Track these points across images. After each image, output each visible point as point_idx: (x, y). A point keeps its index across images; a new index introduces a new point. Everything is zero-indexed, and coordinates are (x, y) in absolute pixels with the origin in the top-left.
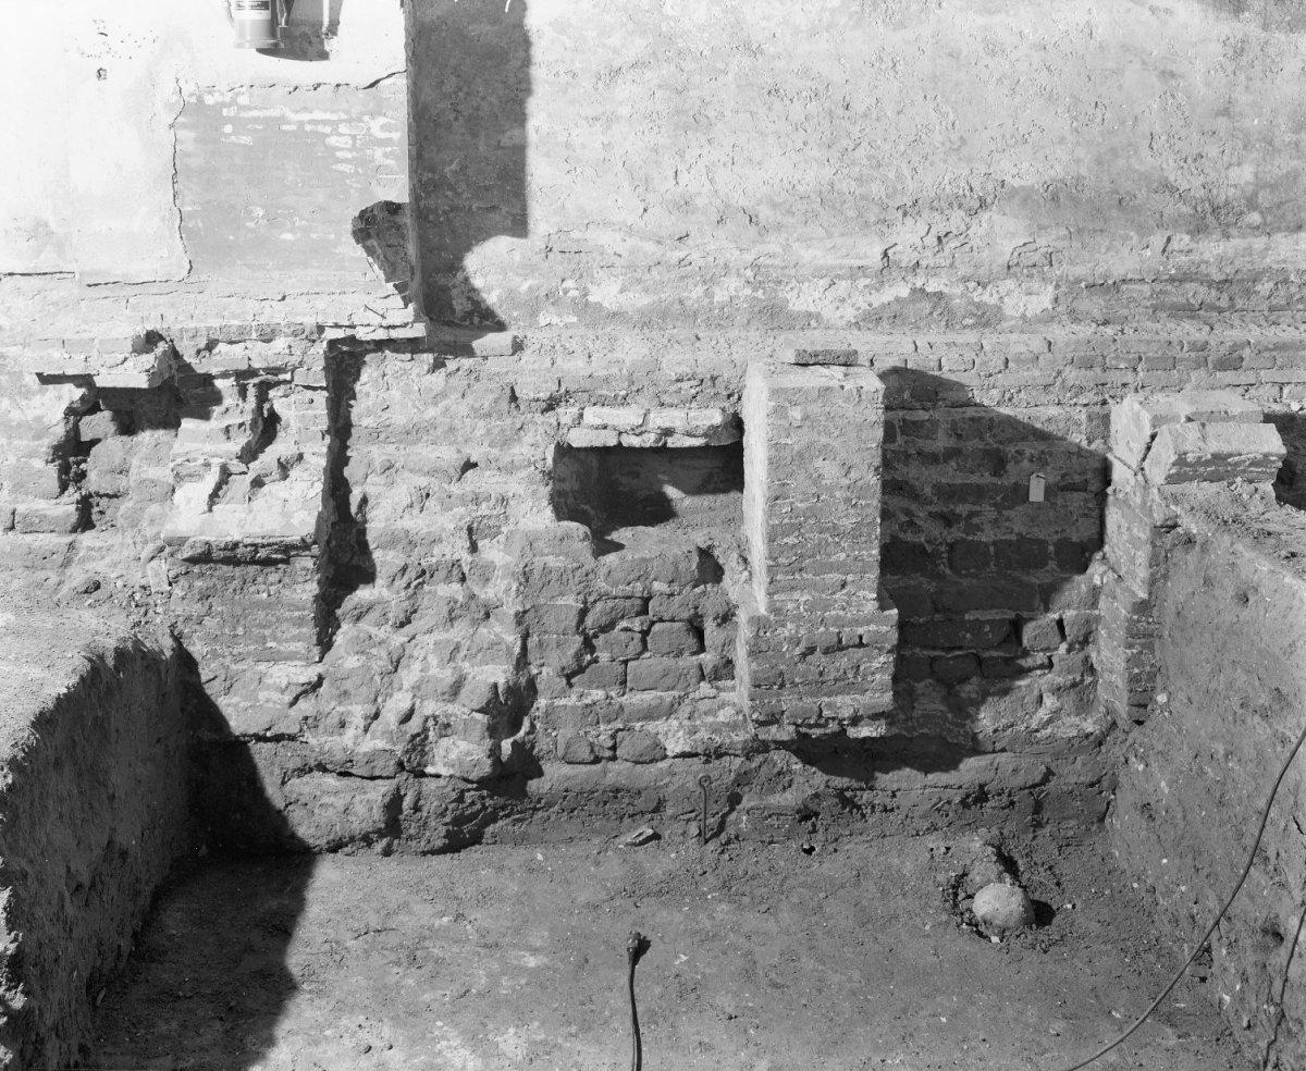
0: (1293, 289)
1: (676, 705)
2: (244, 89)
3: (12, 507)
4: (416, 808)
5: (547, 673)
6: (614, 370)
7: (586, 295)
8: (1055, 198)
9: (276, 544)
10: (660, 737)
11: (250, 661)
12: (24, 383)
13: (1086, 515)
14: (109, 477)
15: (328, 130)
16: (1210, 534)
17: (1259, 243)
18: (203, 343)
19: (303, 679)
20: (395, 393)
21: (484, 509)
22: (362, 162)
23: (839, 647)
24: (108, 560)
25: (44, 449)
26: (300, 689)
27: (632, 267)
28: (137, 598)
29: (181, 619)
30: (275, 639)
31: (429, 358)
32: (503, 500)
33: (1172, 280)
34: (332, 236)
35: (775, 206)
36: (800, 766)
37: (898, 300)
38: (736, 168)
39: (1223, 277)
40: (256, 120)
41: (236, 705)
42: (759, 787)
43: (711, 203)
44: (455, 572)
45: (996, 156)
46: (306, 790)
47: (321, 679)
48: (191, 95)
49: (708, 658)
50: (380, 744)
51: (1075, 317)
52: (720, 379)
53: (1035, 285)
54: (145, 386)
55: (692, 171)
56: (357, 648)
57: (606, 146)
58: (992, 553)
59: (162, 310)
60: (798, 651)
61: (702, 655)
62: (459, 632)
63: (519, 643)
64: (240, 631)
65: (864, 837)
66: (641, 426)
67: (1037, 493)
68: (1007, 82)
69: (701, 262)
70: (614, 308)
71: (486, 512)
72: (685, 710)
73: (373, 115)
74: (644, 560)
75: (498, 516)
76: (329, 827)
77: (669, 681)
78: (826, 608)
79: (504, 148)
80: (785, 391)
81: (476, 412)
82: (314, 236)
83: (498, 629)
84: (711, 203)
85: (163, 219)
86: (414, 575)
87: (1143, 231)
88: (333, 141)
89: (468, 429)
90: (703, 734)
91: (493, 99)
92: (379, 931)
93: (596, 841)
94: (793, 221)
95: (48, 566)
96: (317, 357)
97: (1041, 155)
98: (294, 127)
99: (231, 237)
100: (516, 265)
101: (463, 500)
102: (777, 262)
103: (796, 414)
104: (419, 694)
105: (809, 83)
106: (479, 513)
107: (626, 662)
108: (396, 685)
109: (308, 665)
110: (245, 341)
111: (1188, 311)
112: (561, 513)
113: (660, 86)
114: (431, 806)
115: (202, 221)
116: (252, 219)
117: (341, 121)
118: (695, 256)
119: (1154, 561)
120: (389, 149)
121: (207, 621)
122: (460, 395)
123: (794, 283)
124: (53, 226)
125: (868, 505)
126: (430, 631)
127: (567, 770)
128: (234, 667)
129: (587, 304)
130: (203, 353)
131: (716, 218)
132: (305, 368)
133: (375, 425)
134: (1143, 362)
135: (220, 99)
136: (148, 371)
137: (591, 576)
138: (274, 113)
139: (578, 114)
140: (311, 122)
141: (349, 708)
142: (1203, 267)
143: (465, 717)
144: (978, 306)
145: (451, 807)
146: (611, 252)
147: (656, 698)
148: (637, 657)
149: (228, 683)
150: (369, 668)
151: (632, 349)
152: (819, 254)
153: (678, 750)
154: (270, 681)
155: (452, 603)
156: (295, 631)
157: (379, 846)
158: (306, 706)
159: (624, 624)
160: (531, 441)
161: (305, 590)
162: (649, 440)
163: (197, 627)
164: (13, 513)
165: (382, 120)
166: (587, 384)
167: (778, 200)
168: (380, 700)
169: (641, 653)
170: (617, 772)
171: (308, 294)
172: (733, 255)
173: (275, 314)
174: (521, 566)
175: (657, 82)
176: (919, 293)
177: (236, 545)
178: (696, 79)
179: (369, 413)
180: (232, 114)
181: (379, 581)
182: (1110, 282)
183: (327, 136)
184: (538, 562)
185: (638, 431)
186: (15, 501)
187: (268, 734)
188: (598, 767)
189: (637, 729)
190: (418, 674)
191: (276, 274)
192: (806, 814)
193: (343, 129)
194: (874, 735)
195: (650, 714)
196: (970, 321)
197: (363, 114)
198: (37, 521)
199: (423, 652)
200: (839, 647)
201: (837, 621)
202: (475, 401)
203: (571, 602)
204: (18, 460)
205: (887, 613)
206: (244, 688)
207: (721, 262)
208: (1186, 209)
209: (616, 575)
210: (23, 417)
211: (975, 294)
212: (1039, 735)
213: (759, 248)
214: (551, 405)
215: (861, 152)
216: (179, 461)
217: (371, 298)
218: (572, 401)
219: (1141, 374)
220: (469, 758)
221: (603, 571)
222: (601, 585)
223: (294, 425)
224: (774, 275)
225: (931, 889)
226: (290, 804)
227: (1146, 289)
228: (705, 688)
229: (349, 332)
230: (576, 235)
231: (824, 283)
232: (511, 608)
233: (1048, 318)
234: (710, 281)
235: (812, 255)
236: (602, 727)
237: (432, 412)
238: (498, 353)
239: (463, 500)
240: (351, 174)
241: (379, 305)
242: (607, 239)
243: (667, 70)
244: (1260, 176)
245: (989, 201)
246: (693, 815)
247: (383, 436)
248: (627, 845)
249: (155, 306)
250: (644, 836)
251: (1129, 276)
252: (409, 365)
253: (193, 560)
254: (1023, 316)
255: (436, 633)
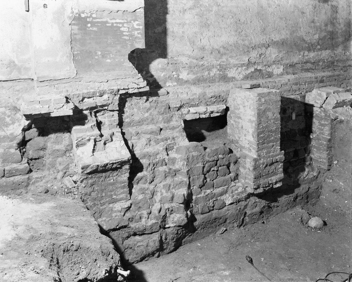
0: (326, 64)
1: (227, 190)
2: (94, 12)
3: (3, 168)
4: (166, 239)
5: (195, 188)
6: (195, 96)
7: (179, 76)
8: (283, 43)
9: (120, 162)
10: (224, 200)
11: (107, 204)
12: (6, 121)
13: (303, 121)
14: (36, 152)
15: (121, 25)
16: (349, 119)
17: (320, 53)
18: (81, 98)
19: (126, 206)
20: (135, 110)
21: (169, 142)
22: (131, 36)
23: (272, 164)
24: (44, 181)
25: (15, 145)
26: (126, 210)
27: (190, 67)
28: (66, 191)
29: (84, 195)
30: (115, 195)
31: (145, 98)
32: (173, 138)
33: (305, 63)
34: (122, 60)
35: (224, 48)
36: (258, 200)
37: (252, 72)
38: (215, 37)
39: (314, 62)
40: (98, 22)
41: (105, 220)
42: (249, 208)
43: (209, 48)
44: (164, 163)
45: (271, 33)
46: (131, 243)
47: (131, 204)
48: (76, 14)
49: (232, 175)
50: (154, 221)
51: (288, 73)
52: (221, 96)
53: (279, 66)
54: (72, 114)
55: (205, 39)
56: (141, 192)
57: (183, 32)
58: (285, 134)
59: (67, 88)
60: (264, 166)
61: (230, 174)
62: (169, 180)
63: (188, 180)
64: (104, 195)
65: (273, 216)
66: (206, 111)
67: (294, 117)
68: (272, 14)
69: (207, 65)
70: (186, 79)
71: (170, 143)
72: (230, 191)
73: (134, 21)
74: (216, 149)
75: (173, 143)
76: (141, 253)
77: (225, 183)
78: (269, 153)
79: (156, 33)
80: (261, 94)
81: (160, 113)
82: (117, 60)
83: (180, 177)
84: (209, 48)
85: (67, 57)
86: (152, 166)
87: (300, 51)
88: (122, 29)
89: (157, 118)
90: (235, 197)
91: (153, 18)
92: (176, 279)
93: (211, 235)
94: (228, 52)
95: (21, 187)
96: (116, 100)
97: (280, 33)
98: (110, 25)
99: (90, 62)
100: (160, 68)
101: (163, 140)
102: (225, 64)
103: (263, 100)
104: (162, 203)
105: (231, 14)
106: (168, 143)
107: (213, 180)
108: (154, 201)
109: (126, 201)
110: (93, 97)
111: (307, 70)
112: (190, 140)
113: (196, 15)
114: (170, 237)
115: (81, 57)
116: (97, 56)
117: (124, 23)
118: (206, 63)
119: (332, 128)
120: (139, 32)
121: (93, 194)
122: (154, 108)
123: (229, 69)
124: (17, 62)
125: (278, 123)
126: (161, 182)
127: (202, 216)
128: (101, 208)
129: (179, 79)
130: (80, 102)
131: (211, 52)
132: (113, 104)
133: (129, 121)
134: (307, 83)
135: (86, 15)
136: (72, 109)
137: (204, 156)
138: (104, 20)
139: (176, 23)
140: (116, 23)
141: (142, 212)
142: (310, 59)
143: (177, 206)
144: (269, 72)
145: (175, 236)
146: (185, 63)
147: (222, 189)
148: (216, 178)
149: (100, 214)
150: (146, 198)
151: (197, 91)
152: (234, 61)
153: (230, 203)
154: (116, 209)
155: (165, 172)
156: (122, 191)
157: (157, 255)
158: (128, 215)
159: (212, 169)
160: (175, 120)
161: (125, 176)
162: (207, 115)
163: (89, 196)
164: (4, 171)
165: (137, 22)
166: (188, 101)
167: (225, 46)
168: (150, 207)
169: (217, 177)
170: (215, 214)
171: (115, 79)
172: (215, 62)
173: (105, 87)
174: (186, 156)
175: (195, 13)
176: (256, 69)
177: (107, 165)
178: (205, 13)
179: (128, 117)
180: (90, 20)
181: (144, 170)
182: (294, 64)
183: (121, 27)
184: (191, 154)
185: (205, 113)
186: (4, 166)
187: (117, 227)
188: (210, 213)
189: (219, 199)
190: (160, 196)
191: (105, 73)
192: (261, 212)
193: (125, 25)
194: (280, 186)
195: (222, 194)
196: (267, 76)
197: (131, 20)
198: (14, 171)
199: (160, 189)
200: (272, 164)
201: (272, 156)
202: (159, 110)
203: (200, 165)
204: (5, 150)
205: (282, 152)
206: (106, 214)
207: (212, 64)
208: (307, 45)
209: (211, 155)
210: (6, 134)
211: (267, 69)
212: (305, 179)
213: (220, 60)
214: (179, 109)
215: (243, 33)
216: (79, 140)
217: (134, 79)
218: (184, 107)
219: (306, 86)
220: (181, 219)
221: (207, 154)
222: (207, 158)
223: (107, 123)
224: (224, 67)
225: (298, 224)
226: (125, 249)
227: (300, 65)
228: (233, 184)
229: (126, 91)
230: (175, 58)
231: (235, 68)
232: (185, 170)
233: (282, 74)
234: (209, 70)
235: (233, 61)
236: (210, 201)
237: (147, 115)
238: (163, 94)
239: (163, 140)
240: (128, 40)
241: (137, 81)
242: (184, 60)
243: (198, 10)
244: (320, 37)
245: (270, 45)
246: (234, 221)
247: (132, 124)
248: (220, 234)
249: (65, 87)
250: (224, 230)
251: (297, 62)
252: (139, 101)
253: (89, 173)
254: (277, 74)
255: (162, 182)
